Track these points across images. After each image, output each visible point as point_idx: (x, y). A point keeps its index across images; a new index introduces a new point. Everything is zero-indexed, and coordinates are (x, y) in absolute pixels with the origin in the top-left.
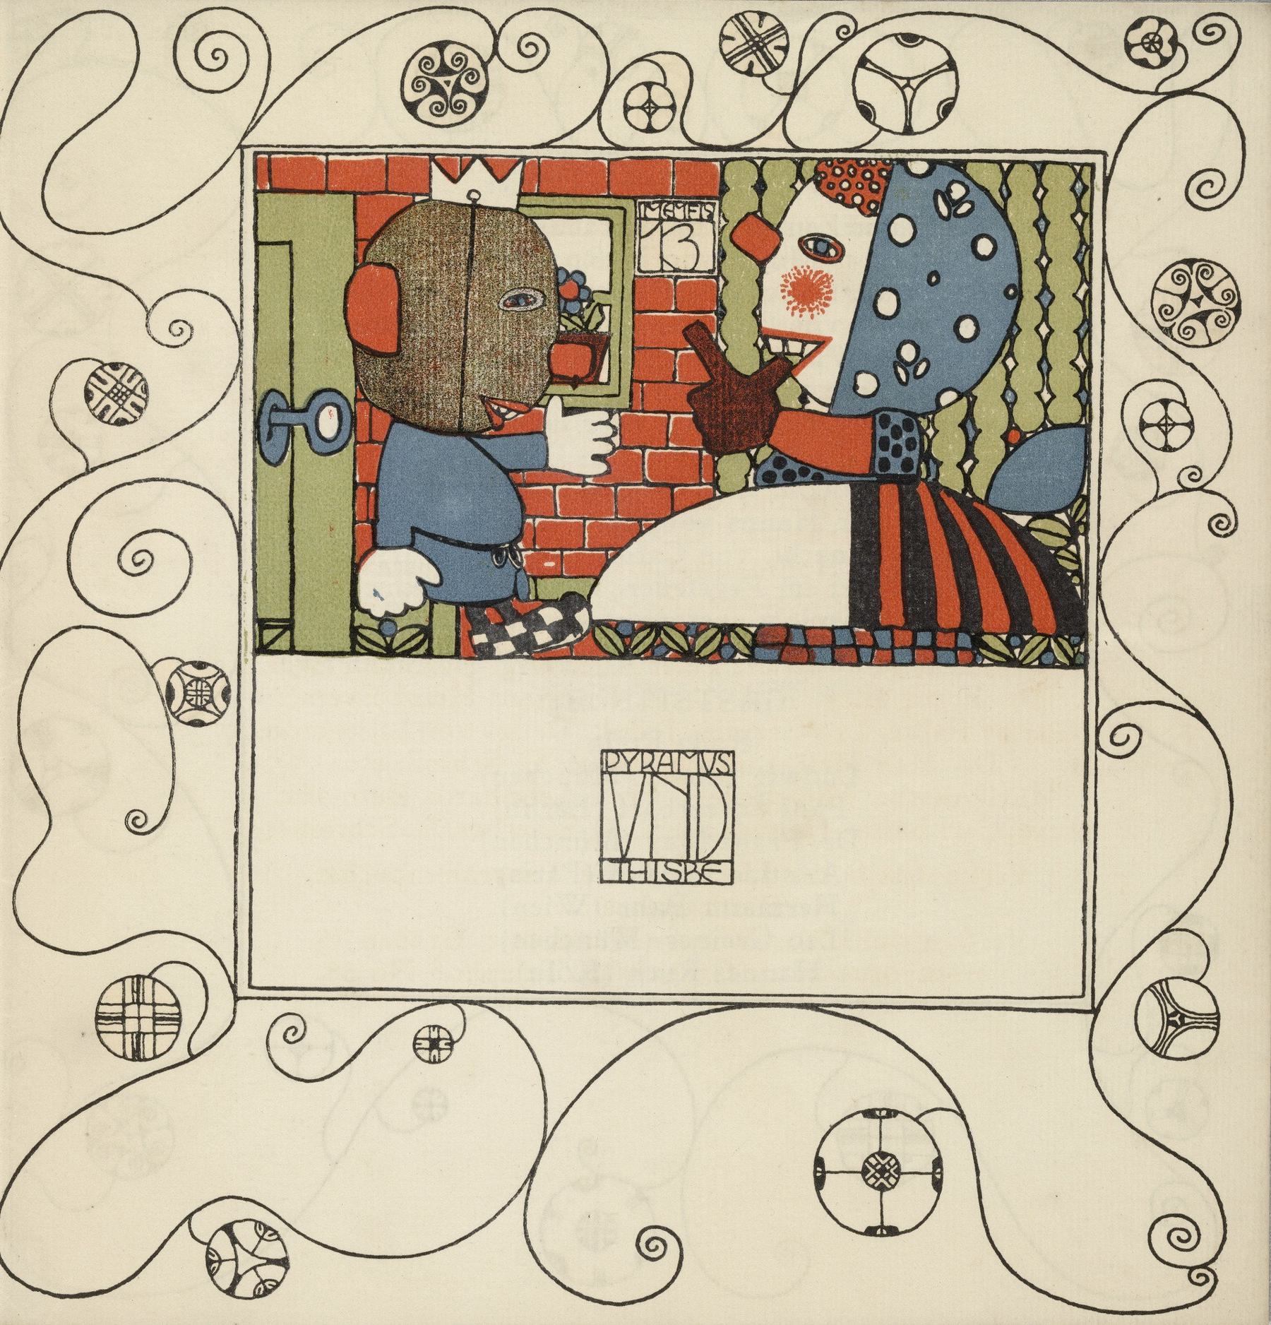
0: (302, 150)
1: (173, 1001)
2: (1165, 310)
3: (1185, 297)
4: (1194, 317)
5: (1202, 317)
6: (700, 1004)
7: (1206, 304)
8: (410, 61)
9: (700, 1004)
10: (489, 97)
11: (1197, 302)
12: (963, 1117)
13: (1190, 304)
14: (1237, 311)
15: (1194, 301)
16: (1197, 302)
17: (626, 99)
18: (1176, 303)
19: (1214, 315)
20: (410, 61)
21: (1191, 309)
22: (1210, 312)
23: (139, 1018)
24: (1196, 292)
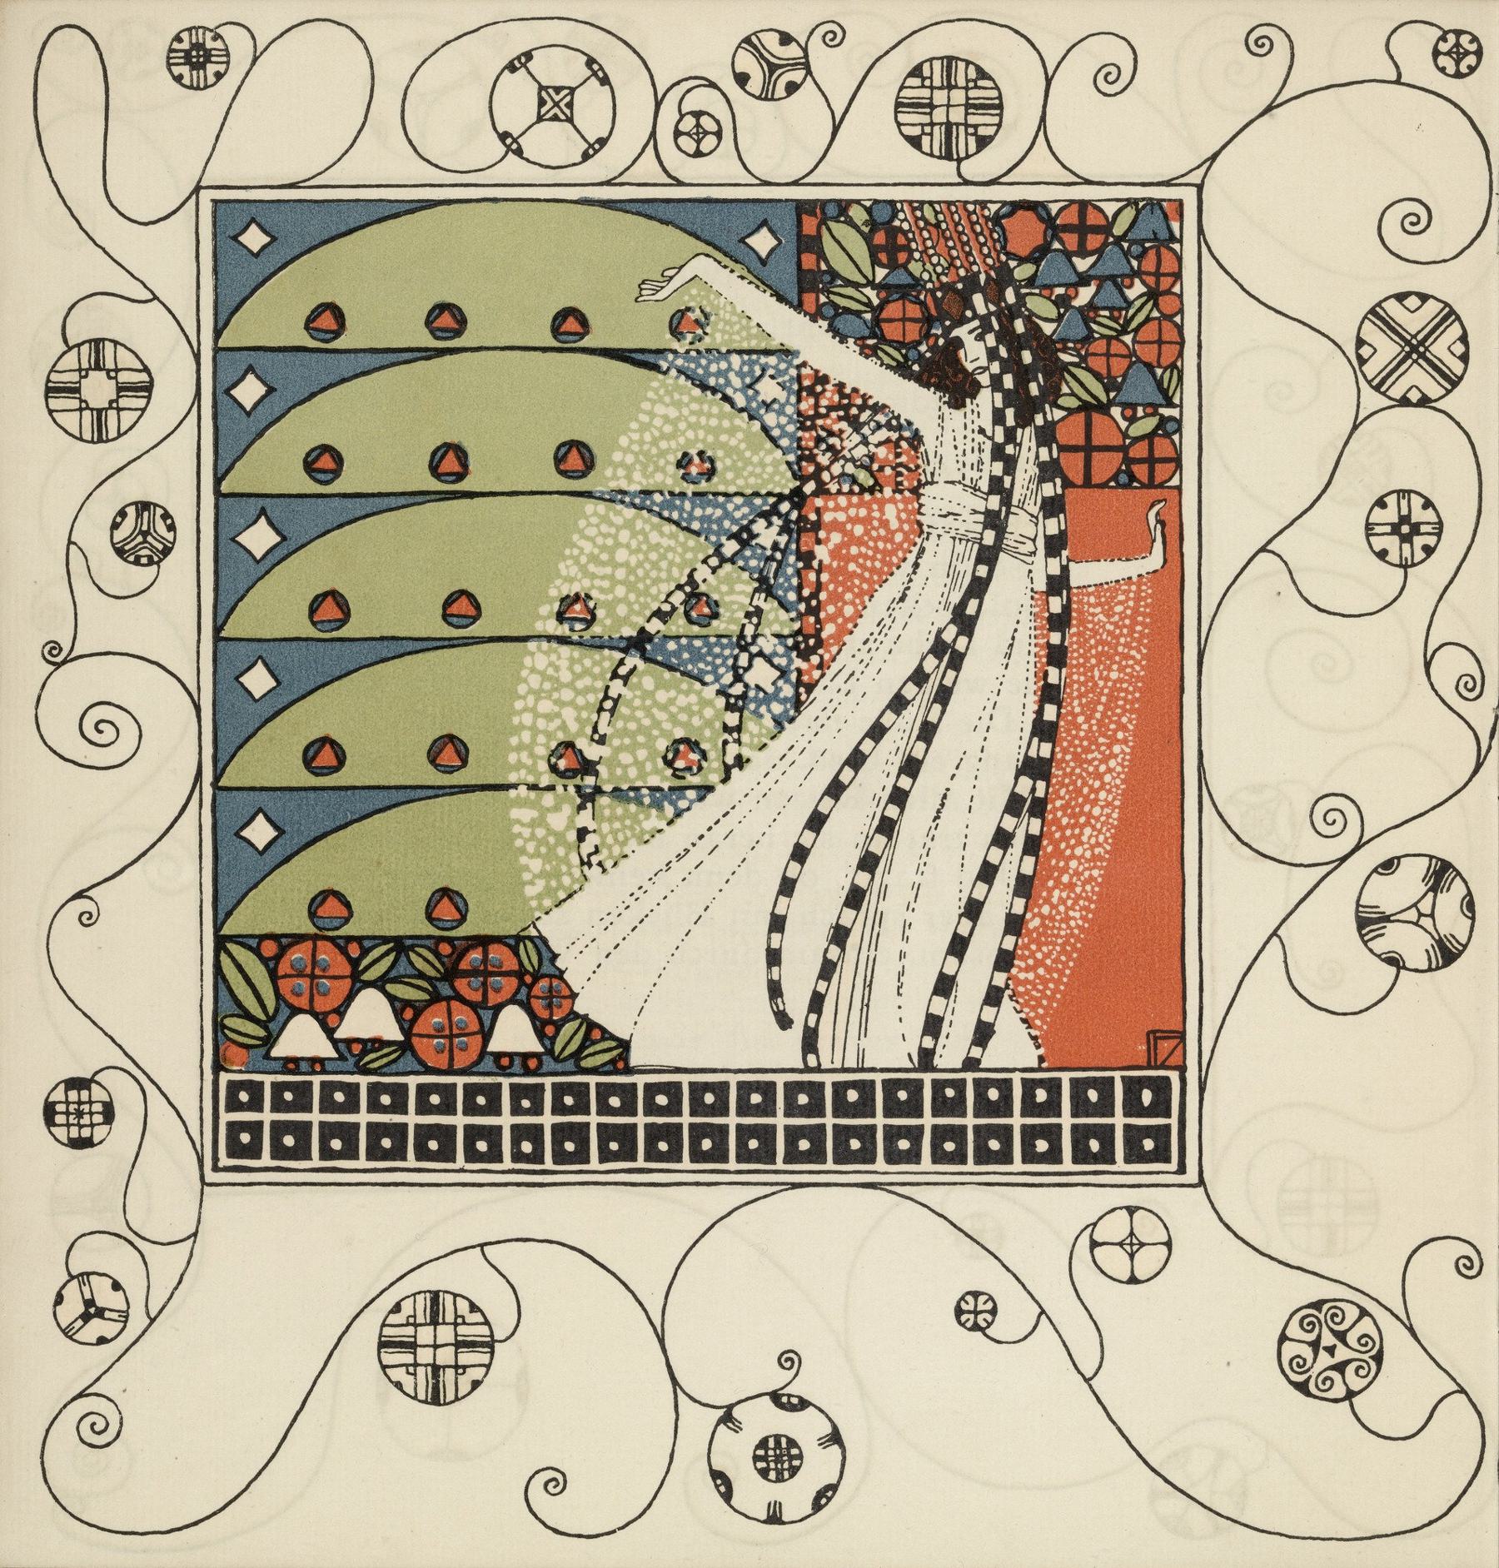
0: (1384, 374)
1: (72, 547)
2: (1299, 1363)
3: (1315, 1345)
4: (1319, 1337)
5: (1340, 1368)
6: (772, 1184)
7: (1342, 1353)
8: (678, 83)
9: (772, 1184)
10: (697, 109)
11: (1331, 1350)
12: (836, 129)
13: (1323, 1354)
14: (1379, 1358)
15: (1326, 1349)
16: (1331, 1350)
17: (495, 129)
18: (1307, 1352)
19: (1354, 1365)
20: (678, 83)
21: (1324, 1360)
22: (1348, 1362)
23: (948, 106)
24: (1328, 1339)
